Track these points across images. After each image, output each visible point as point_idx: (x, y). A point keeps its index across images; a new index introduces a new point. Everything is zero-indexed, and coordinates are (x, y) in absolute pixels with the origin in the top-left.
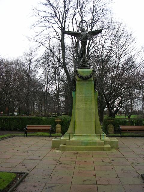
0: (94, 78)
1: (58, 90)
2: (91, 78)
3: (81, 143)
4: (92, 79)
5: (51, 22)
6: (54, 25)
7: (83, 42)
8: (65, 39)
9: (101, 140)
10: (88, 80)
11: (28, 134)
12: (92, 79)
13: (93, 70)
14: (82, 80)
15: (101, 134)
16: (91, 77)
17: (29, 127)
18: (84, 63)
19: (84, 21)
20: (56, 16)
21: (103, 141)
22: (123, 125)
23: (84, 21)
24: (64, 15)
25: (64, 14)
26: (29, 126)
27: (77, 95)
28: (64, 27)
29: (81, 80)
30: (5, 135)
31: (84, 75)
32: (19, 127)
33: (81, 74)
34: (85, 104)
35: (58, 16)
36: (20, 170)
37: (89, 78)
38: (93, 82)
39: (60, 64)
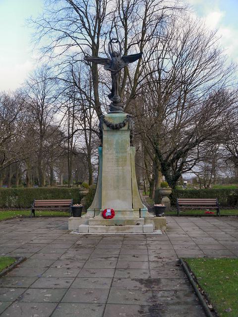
1: (90, 145)
5: (76, 38)
6: (79, 41)
7: (114, 73)
10: (121, 129)
13: (127, 115)
16: (124, 125)
17: (38, 202)
19: (116, 40)
20: (85, 27)
22: (208, 198)
24: (97, 25)
25: (96, 23)
26: (38, 201)
28: (96, 43)
29: (110, 129)
32: (27, 205)
33: (110, 121)
35: (87, 25)
36: (19, 254)
39: (92, 106)
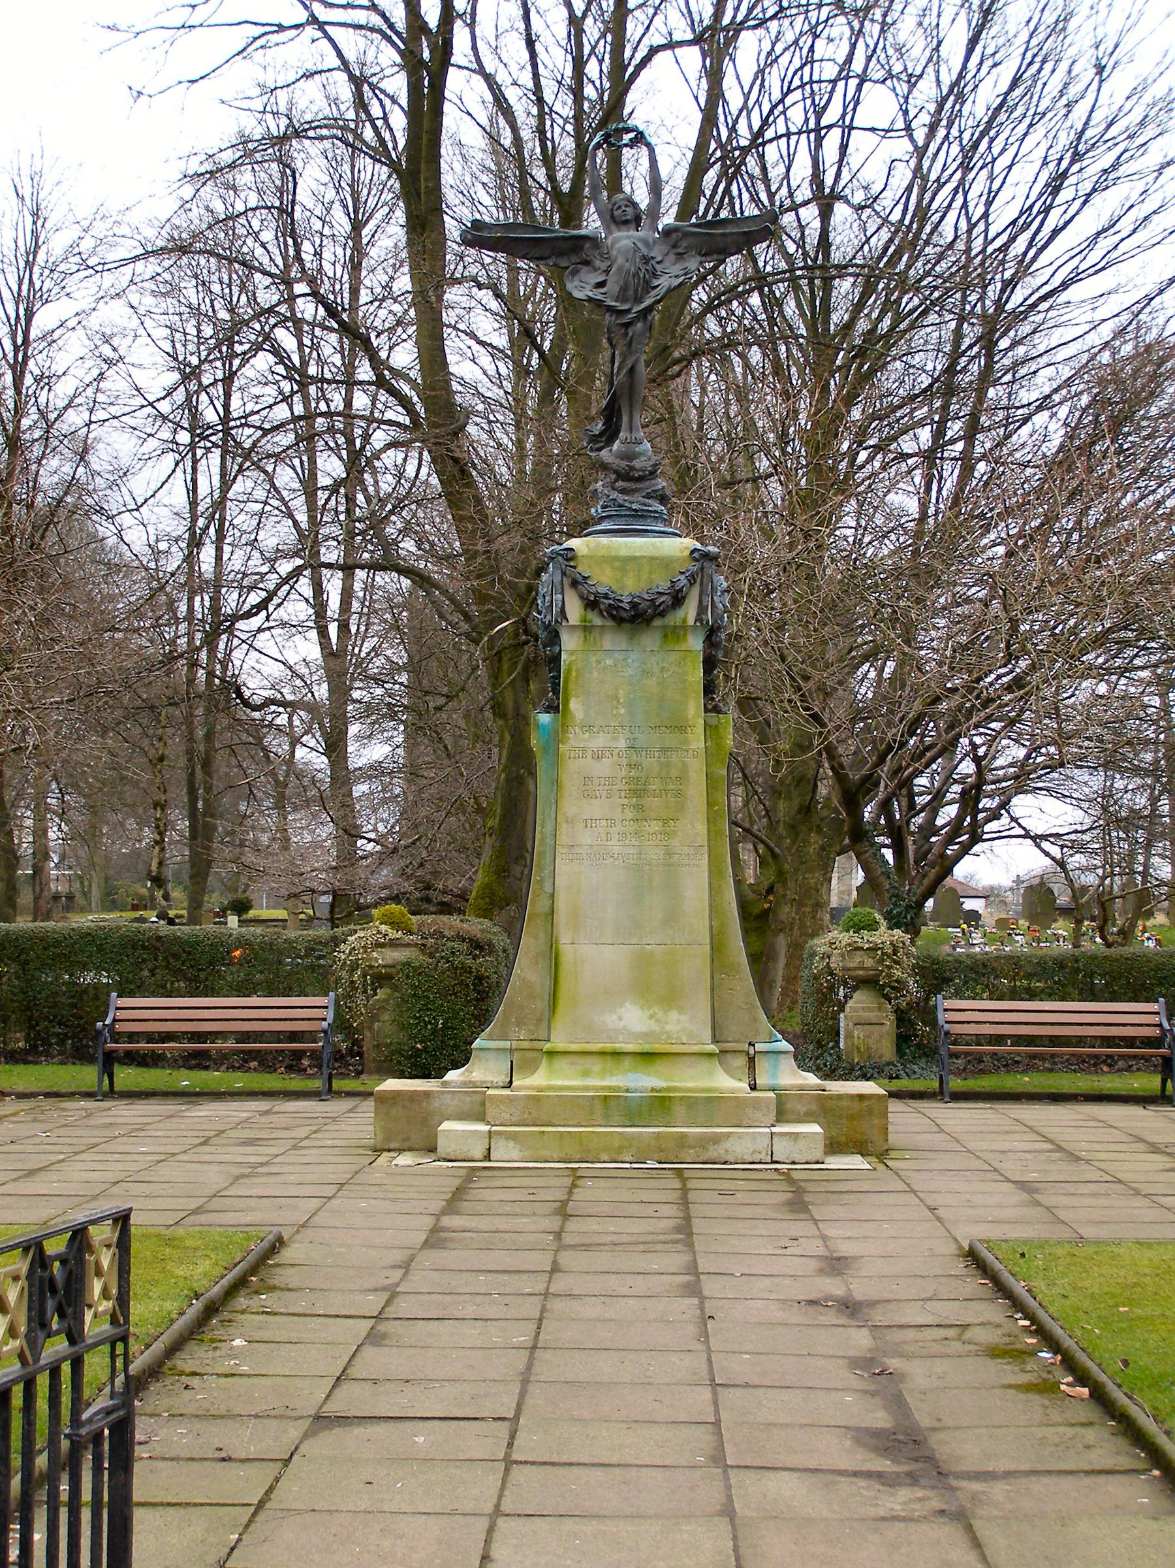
0: (702, 609)
2: (680, 614)
3: (598, 1106)
4: (691, 621)
8: (137, 1467)
9: (753, 1087)
10: (657, 622)
11: (337, 1084)
12: (689, 611)
14: (610, 623)
15: (759, 1047)
16: (678, 599)
18: (623, 491)
19: (632, 135)
21: (771, 1094)
23: (632, 135)
27: (576, 739)
30: (612, 1075)
31: (631, 588)
33: (603, 579)
34: (629, 814)
37: (662, 614)
38: (696, 643)
